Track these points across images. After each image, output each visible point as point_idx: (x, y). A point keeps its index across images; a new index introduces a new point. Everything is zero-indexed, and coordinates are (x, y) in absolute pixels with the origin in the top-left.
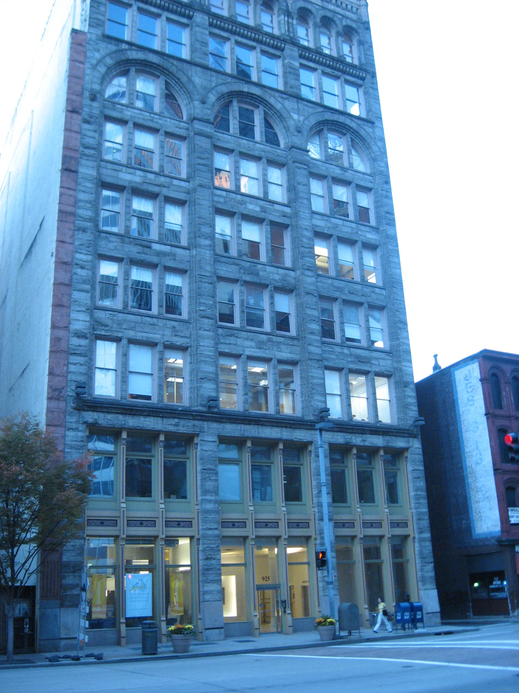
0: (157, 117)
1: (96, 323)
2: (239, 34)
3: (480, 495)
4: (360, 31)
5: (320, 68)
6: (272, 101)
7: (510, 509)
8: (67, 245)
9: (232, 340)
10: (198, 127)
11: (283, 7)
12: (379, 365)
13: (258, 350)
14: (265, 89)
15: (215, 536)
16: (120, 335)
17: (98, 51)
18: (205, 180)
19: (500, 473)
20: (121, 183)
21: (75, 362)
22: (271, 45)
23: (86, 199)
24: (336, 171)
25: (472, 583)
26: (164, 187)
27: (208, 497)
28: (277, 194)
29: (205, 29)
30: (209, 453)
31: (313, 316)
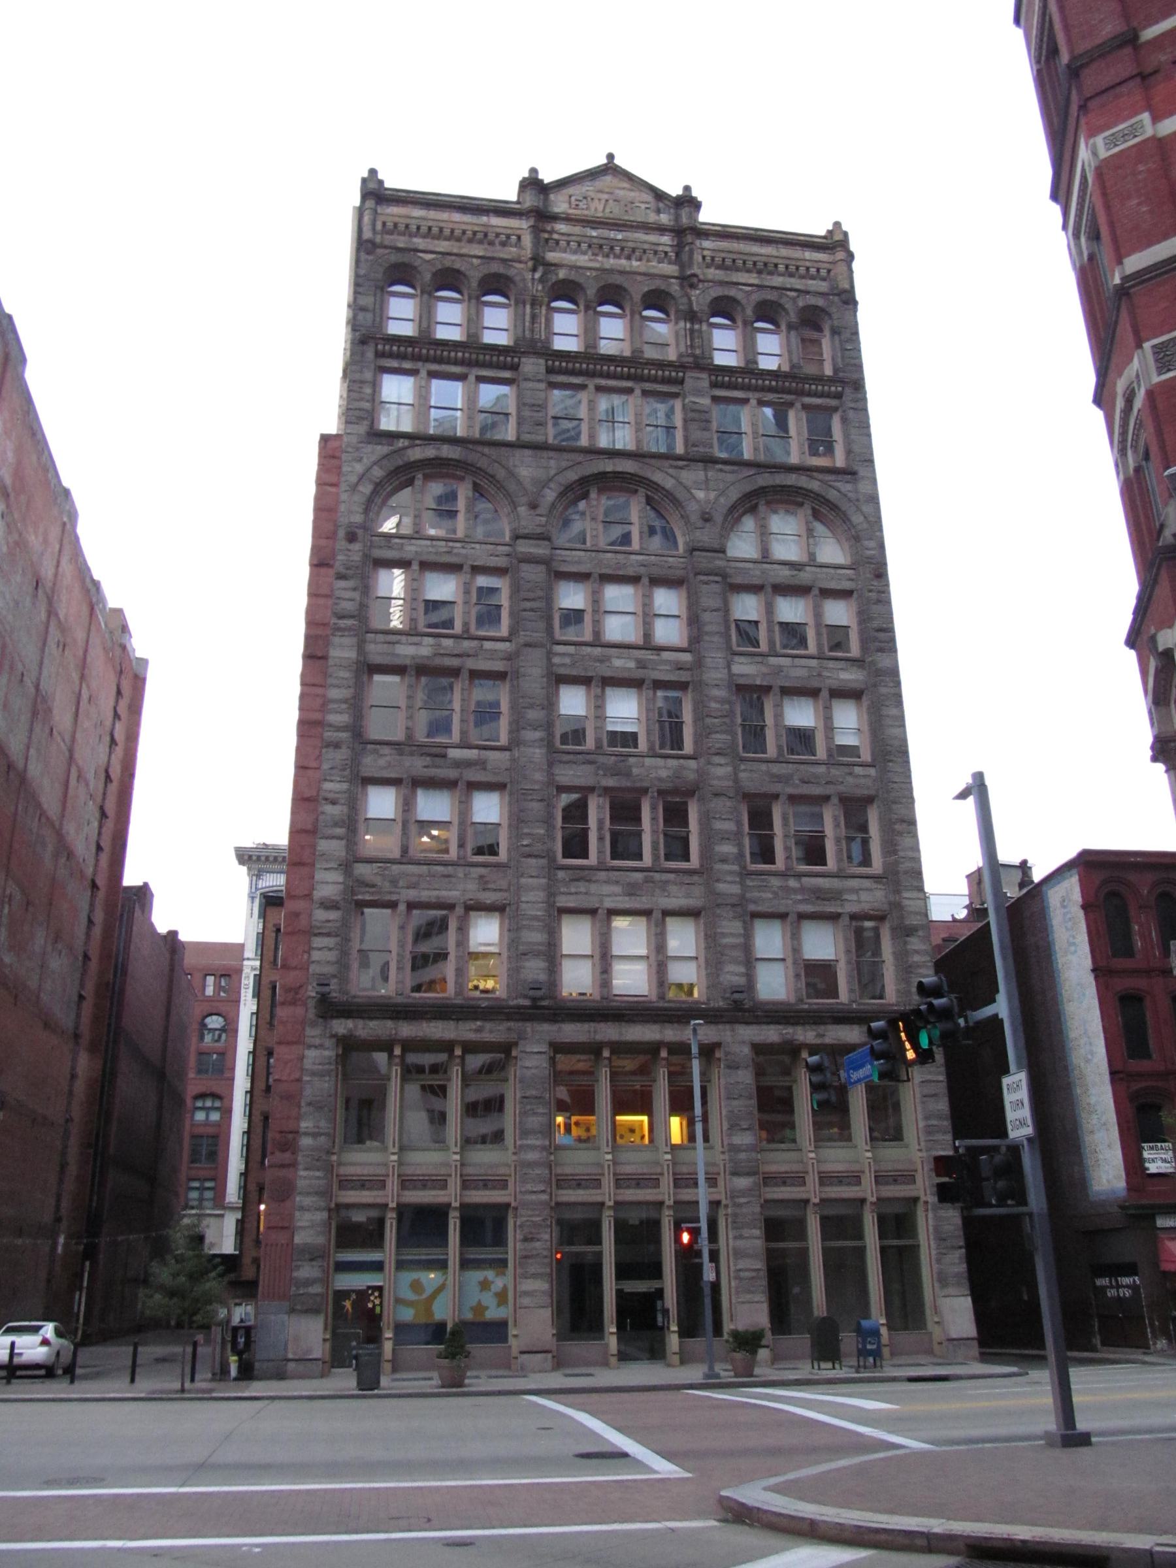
0: (458, 545)
1: (354, 884)
2: (602, 375)
3: (1094, 1119)
4: (833, 310)
5: (753, 397)
6: (658, 477)
7: (1145, 1145)
8: (310, 772)
9: (582, 887)
10: (523, 550)
11: (681, 307)
12: (859, 902)
13: (627, 898)
14: (647, 460)
15: (541, 1203)
16: (394, 898)
17: (360, 460)
18: (535, 634)
19: (1121, 1079)
20: (398, 661)
21: (320, 946)
22: (659, 379)
23: (341, 696)
24: (781, 573)
25: (1053, 1283)
26: (469, 656)
27: (530, 1142)
28: (668, 632)
29: (539, 381)
30: (533, 1071)
31: (726, 832)
